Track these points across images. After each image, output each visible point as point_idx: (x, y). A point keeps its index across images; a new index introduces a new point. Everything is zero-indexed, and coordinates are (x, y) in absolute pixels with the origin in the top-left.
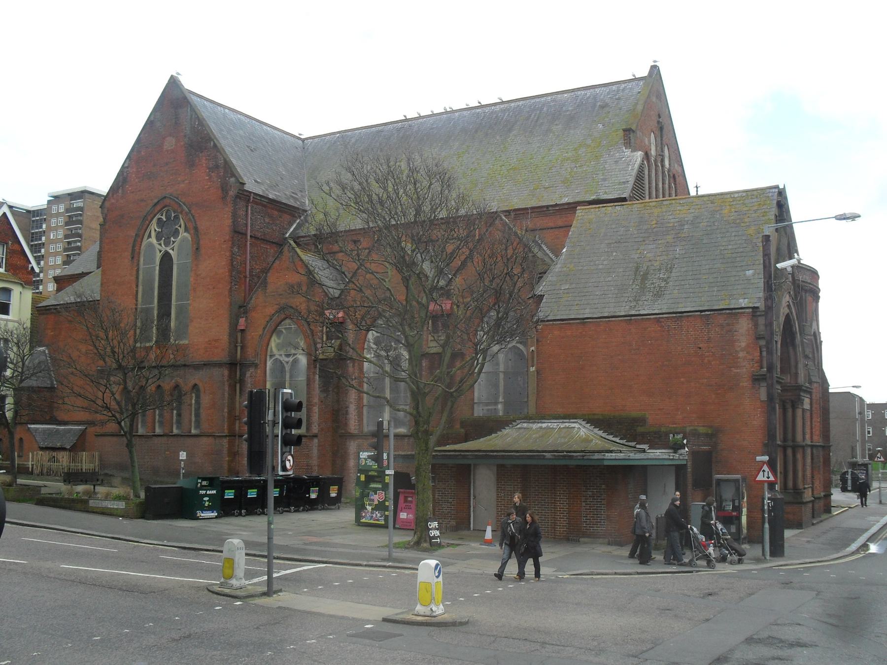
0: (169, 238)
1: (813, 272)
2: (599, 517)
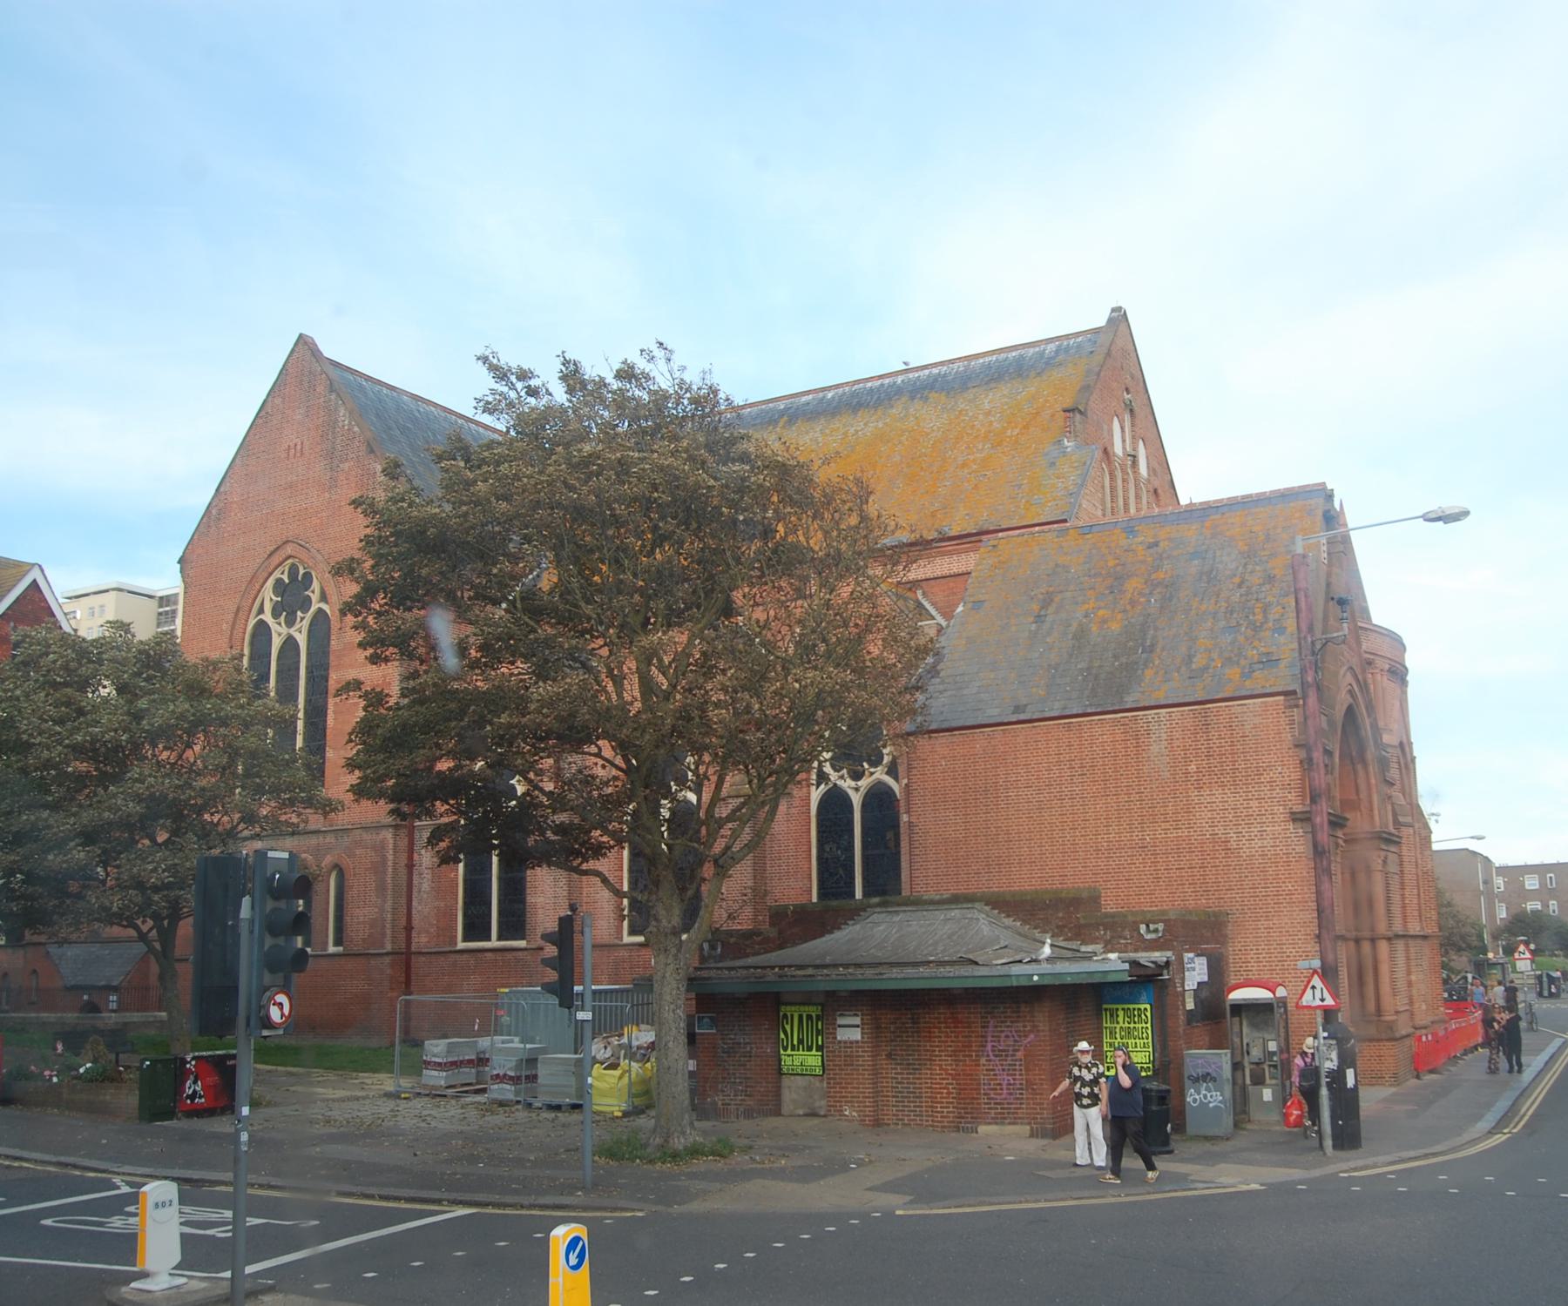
0: (295, 613)
1: (1396, 640)
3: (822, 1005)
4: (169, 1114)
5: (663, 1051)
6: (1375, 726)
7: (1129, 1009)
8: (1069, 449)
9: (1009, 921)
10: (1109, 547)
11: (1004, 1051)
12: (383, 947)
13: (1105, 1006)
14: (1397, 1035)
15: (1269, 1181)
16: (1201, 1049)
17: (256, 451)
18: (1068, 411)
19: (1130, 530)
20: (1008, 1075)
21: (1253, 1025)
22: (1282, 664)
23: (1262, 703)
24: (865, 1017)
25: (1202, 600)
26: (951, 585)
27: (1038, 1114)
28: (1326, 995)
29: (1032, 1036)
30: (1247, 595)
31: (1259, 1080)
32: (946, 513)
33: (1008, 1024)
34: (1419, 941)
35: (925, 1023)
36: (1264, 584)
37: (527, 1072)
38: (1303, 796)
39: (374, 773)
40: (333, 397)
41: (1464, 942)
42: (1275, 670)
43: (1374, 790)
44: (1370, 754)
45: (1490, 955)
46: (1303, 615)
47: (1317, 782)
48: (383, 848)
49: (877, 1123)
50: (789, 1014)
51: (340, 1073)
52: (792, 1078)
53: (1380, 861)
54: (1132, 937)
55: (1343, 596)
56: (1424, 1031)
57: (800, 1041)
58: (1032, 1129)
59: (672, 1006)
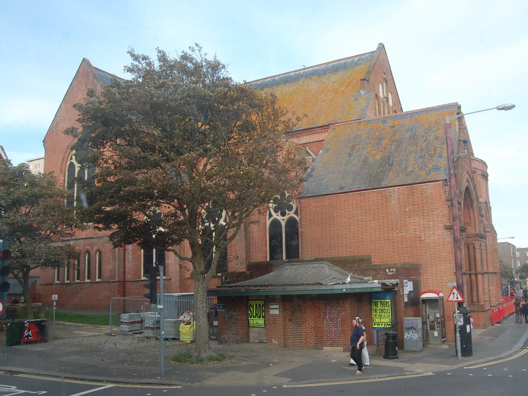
3: (264, 301)
4: (19, 343)
5: (198, 319)
6: (476, 194)
7: (382, 302)
8: (362, 94)
9: (336, 268)
10: (376, 128)
11: (333, 318)
12: (115, 279)
13: (373, 301)
14: (485, 310)
15: (436, 371)
16: (410, 317)
17: (69, 101)
19: (384, 122)
20: (334, 327)
21: (431, 307)
22: (442, 169)
23: (434, 184)
24: (280, 305)
25: (411, 146)
26: (319, 144)
27: (346, 342)
28: (459, 296)
29: (344, 313)
30: (428, 144)
31: (433, 328)
32: (317, 118)
33: (335, 308)
34: (493, 275)
35: (303, 307)
36: (435, 140)
37: (157, 326)
38: (450, 220)
39: (80, 211)
40: (95, 80)
41: (507, 275)
42: (438, 172)
43: (476, 219)
44: (475, 204)
45: (516, 279)
46: (449, 147)
47: (455, 213)
49: (285, 346)
50: (252, 304)
51: (94, 325)
52: (253, 328)
53: (478, 245)
54: (383, 274)
55: (465, 139)
56: (494, 308)
57: (256, 314)
58: (344, 348)
59: (201, 302)
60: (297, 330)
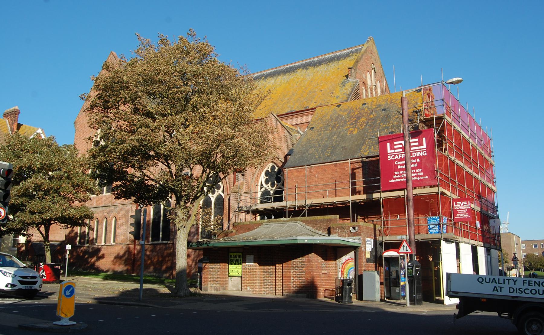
2: (301, 279)
9: (308, 227)
18: (350, 69)
28: (408, 248)
48: (128, 211)
54: (347, 231)
60: (268, 279)
